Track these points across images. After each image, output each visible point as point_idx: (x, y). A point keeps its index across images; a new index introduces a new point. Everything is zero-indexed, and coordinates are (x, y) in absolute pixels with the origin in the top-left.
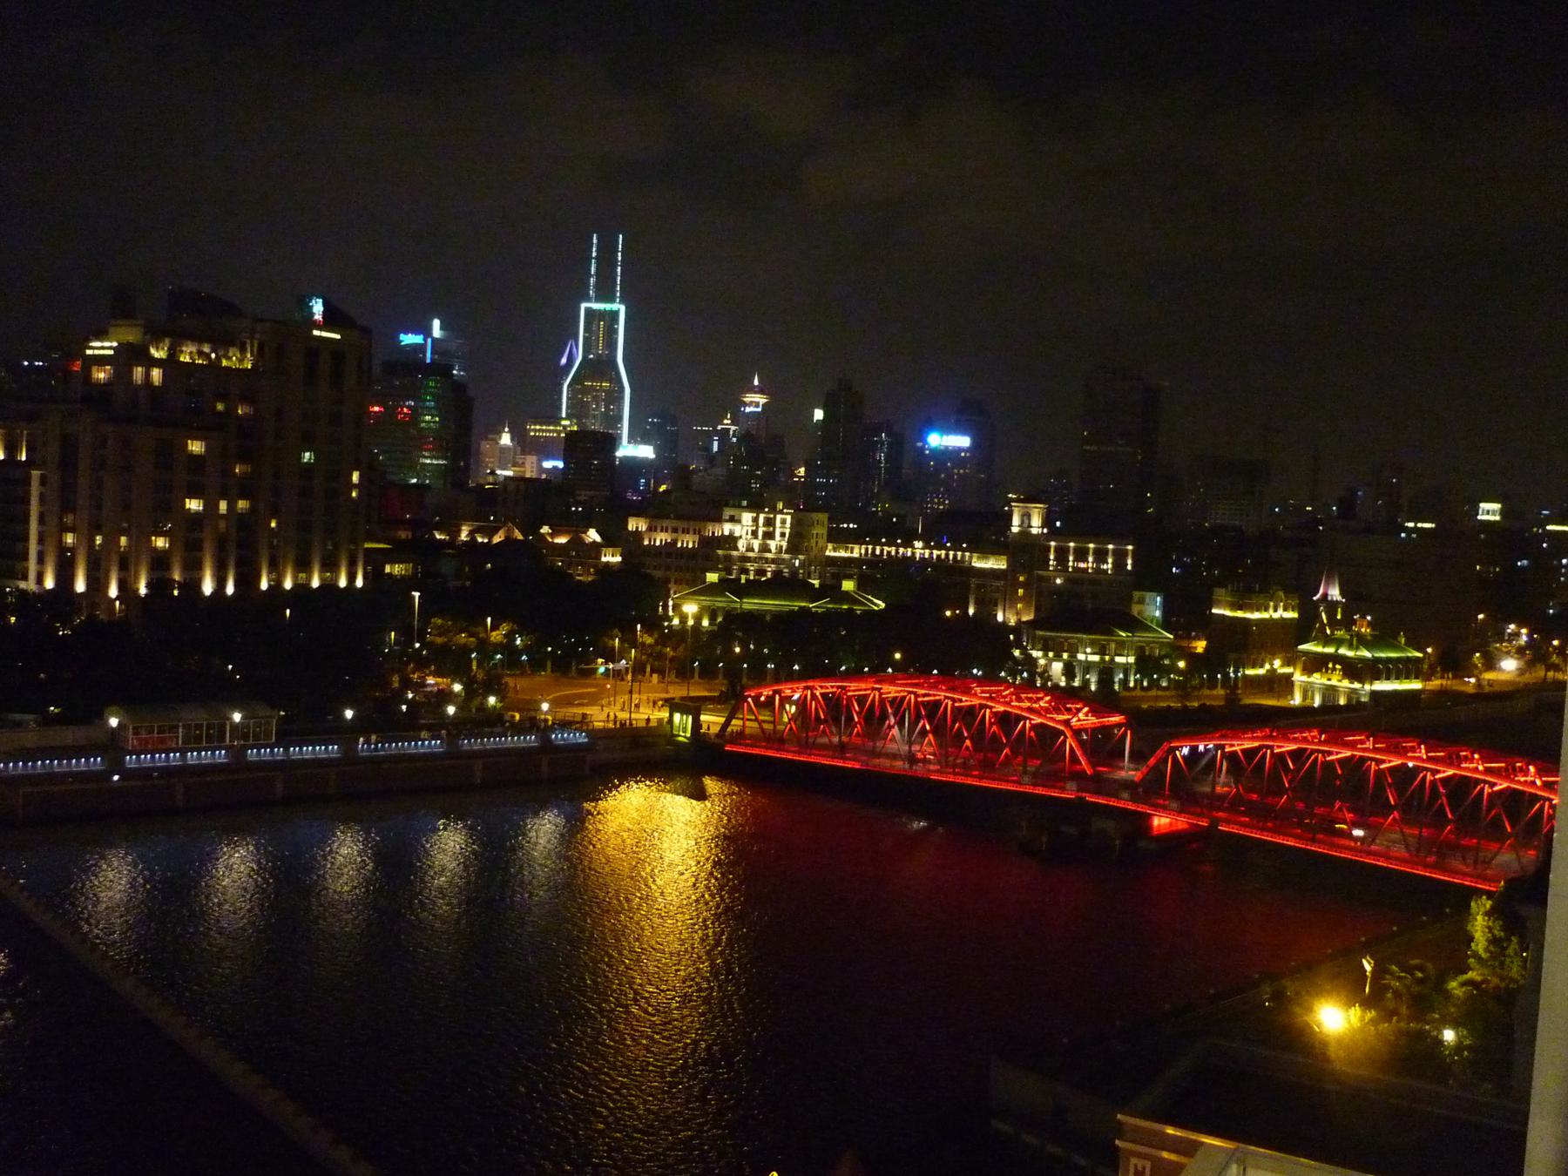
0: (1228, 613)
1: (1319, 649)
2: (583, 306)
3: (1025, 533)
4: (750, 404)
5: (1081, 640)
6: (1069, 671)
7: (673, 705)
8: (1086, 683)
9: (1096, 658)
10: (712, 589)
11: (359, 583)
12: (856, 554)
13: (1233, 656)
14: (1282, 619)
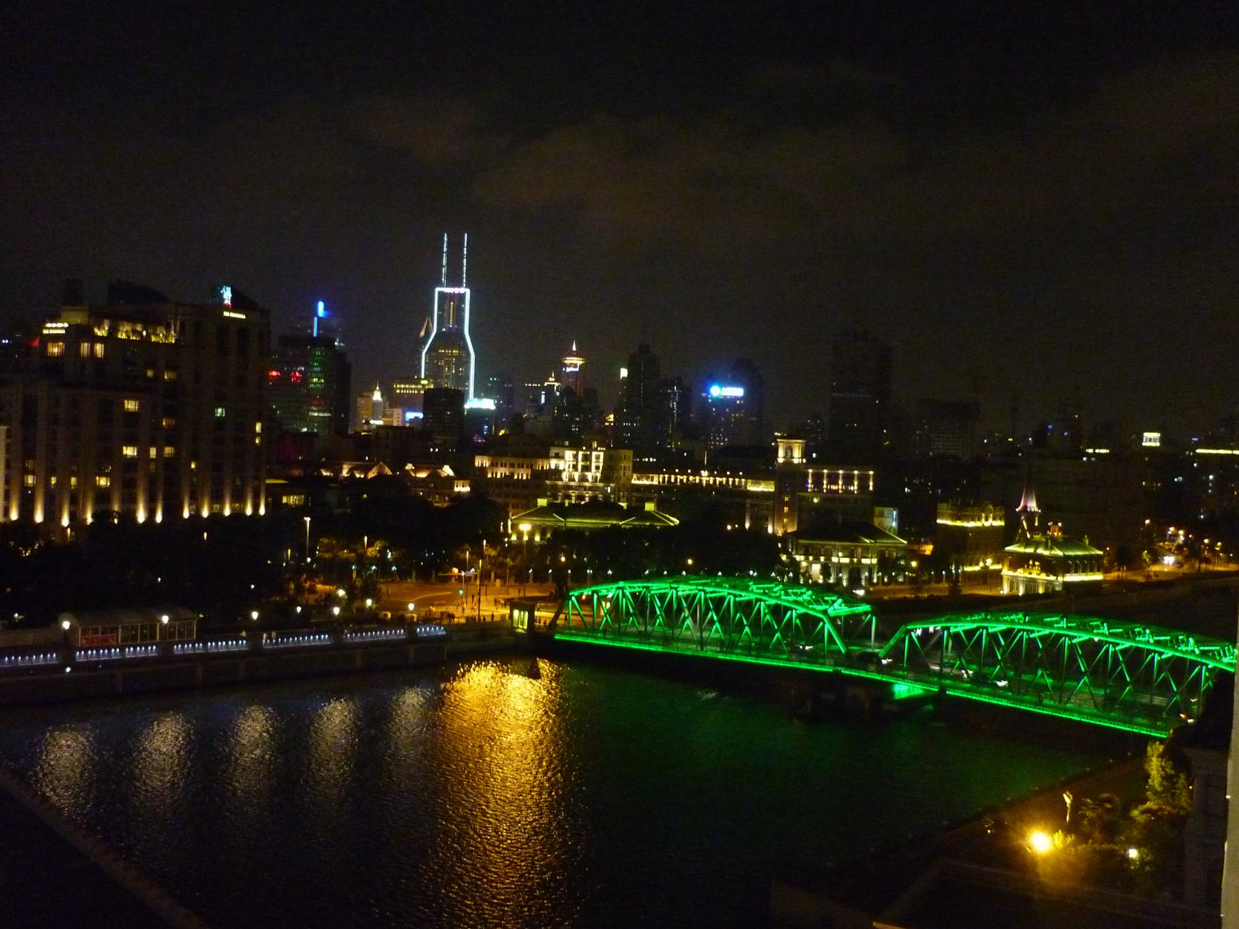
0: (949, 523)
1: (1022, 550)
3: (788, 463)
4: (570, 365)
5: (834, 547)
6: (825, 571)
7: (512, 604)
9: (847, 560)
11: (262, 511)
13: (954, 556)
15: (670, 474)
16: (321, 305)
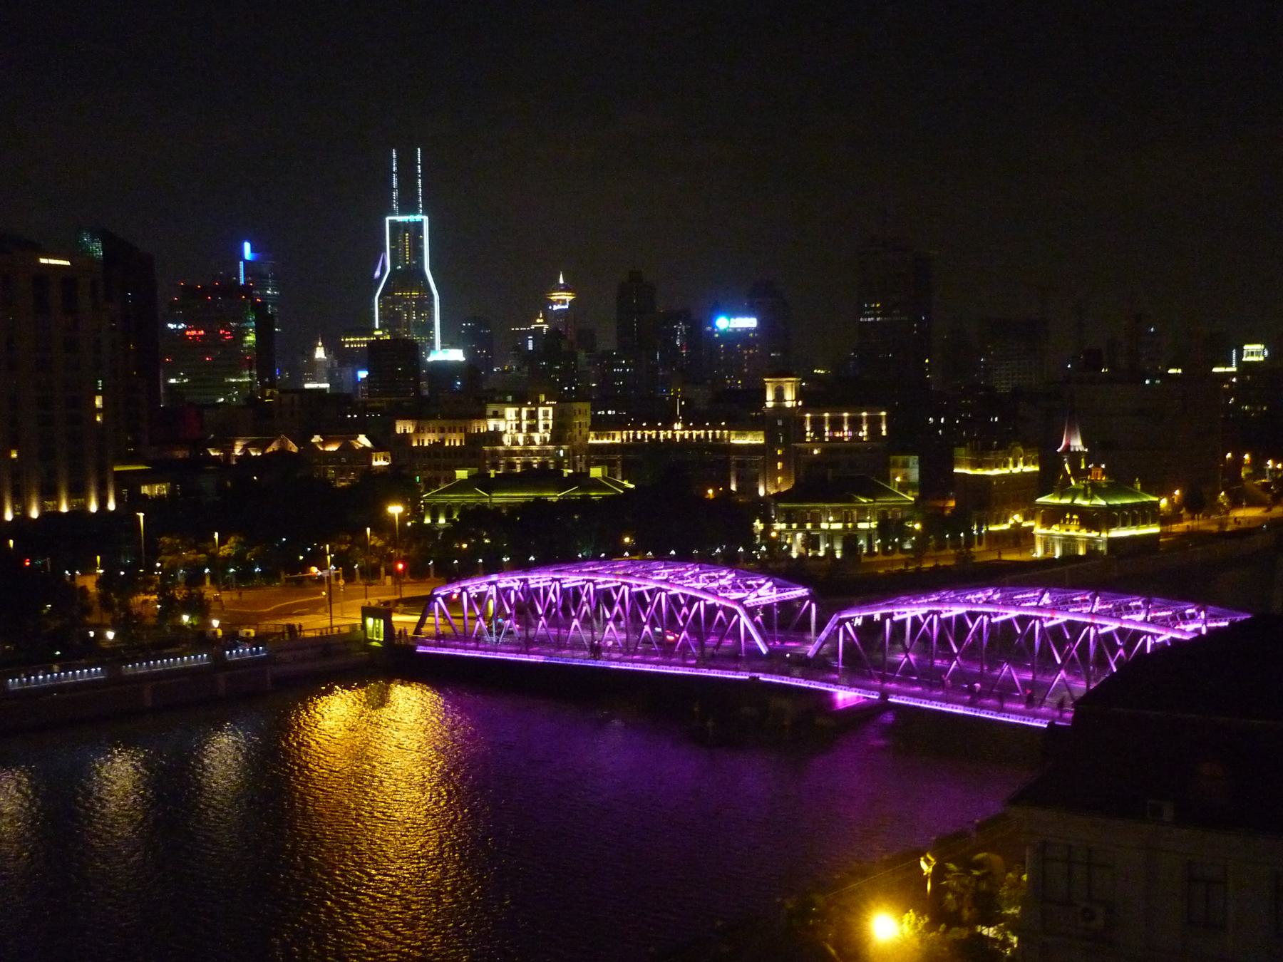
0: (969, 471)
1: (1056, 501)
2: (388, 219)
3: (780, 408)
4: (558, 302)
5: (824, 510)
6: (811, 542)
7: (367, 612)
8: (831, 552)
9: (839, 526)
10: (463, 486)
11: (111, 506)
12: (617, 440)
13: (976, 514)
14: (1023, 474)
15: (635, 430)
16: (247, 246)
